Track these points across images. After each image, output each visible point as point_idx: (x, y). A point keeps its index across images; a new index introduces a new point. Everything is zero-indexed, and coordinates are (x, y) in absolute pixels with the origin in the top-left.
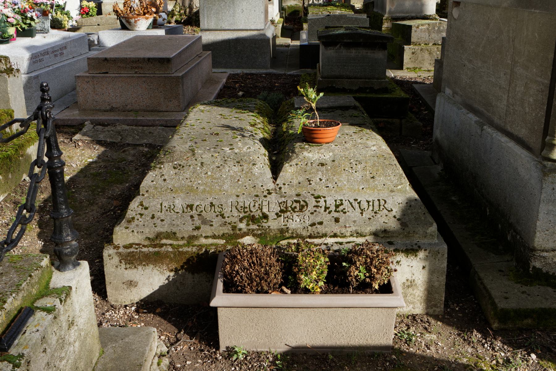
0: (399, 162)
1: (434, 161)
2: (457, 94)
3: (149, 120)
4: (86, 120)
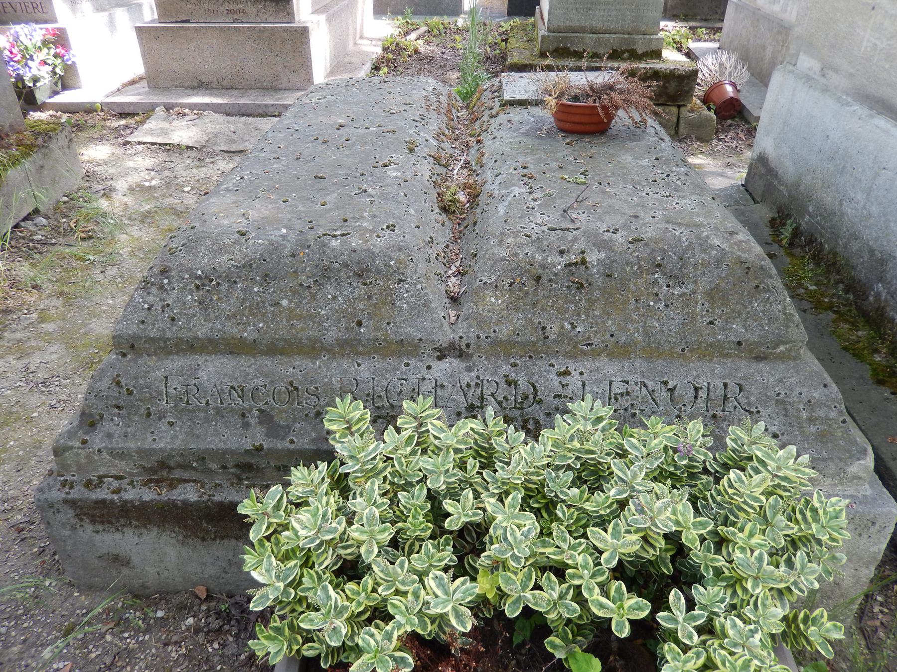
0: (521, 71)
1: (754, 199)
2: (836, 71)
3: (259, 105)
4: (157, 105)
